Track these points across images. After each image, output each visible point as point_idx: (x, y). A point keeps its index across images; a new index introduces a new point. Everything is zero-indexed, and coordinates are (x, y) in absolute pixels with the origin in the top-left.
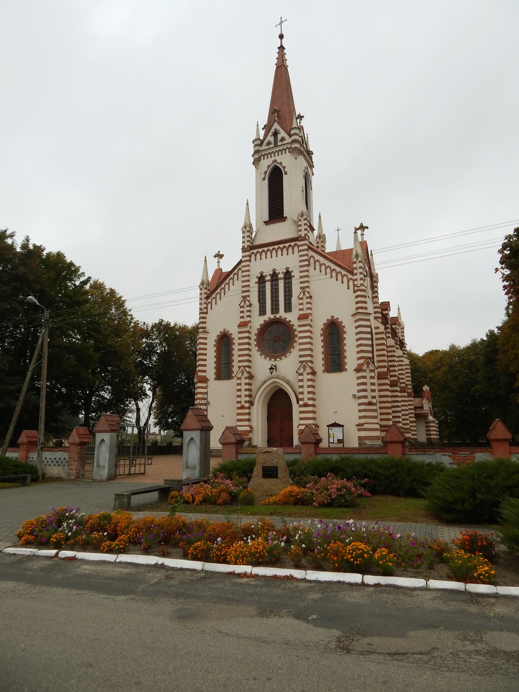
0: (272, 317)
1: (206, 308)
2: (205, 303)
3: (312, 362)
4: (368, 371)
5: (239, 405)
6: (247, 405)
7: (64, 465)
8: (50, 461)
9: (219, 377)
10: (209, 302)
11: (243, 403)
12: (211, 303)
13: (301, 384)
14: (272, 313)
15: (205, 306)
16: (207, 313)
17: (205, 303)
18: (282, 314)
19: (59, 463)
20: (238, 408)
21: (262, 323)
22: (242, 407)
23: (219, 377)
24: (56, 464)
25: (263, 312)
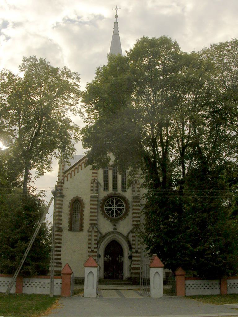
0: (113, 192)
1: (63, 179)
2: (62, 176)
3: (97, 224)
4: (136, 232)
5: (90, 250)
6: (95, 250)
7: (201, 289)
8: (212, 286)
9: (71, 229)
10: (66, 176)
11: (93, 249)
12: (67, 177)
13: (134, 239)
14: (113, 190)
15: (63, 178)
16: (63, 183)
17: (62, 176)
18: (119, 190)
19: (4, 284)
20: (89, 252)
21: (106, 196)
22: (92, 251)
23: (71, 229)
24: (194, 288)
25: (106, 188)
